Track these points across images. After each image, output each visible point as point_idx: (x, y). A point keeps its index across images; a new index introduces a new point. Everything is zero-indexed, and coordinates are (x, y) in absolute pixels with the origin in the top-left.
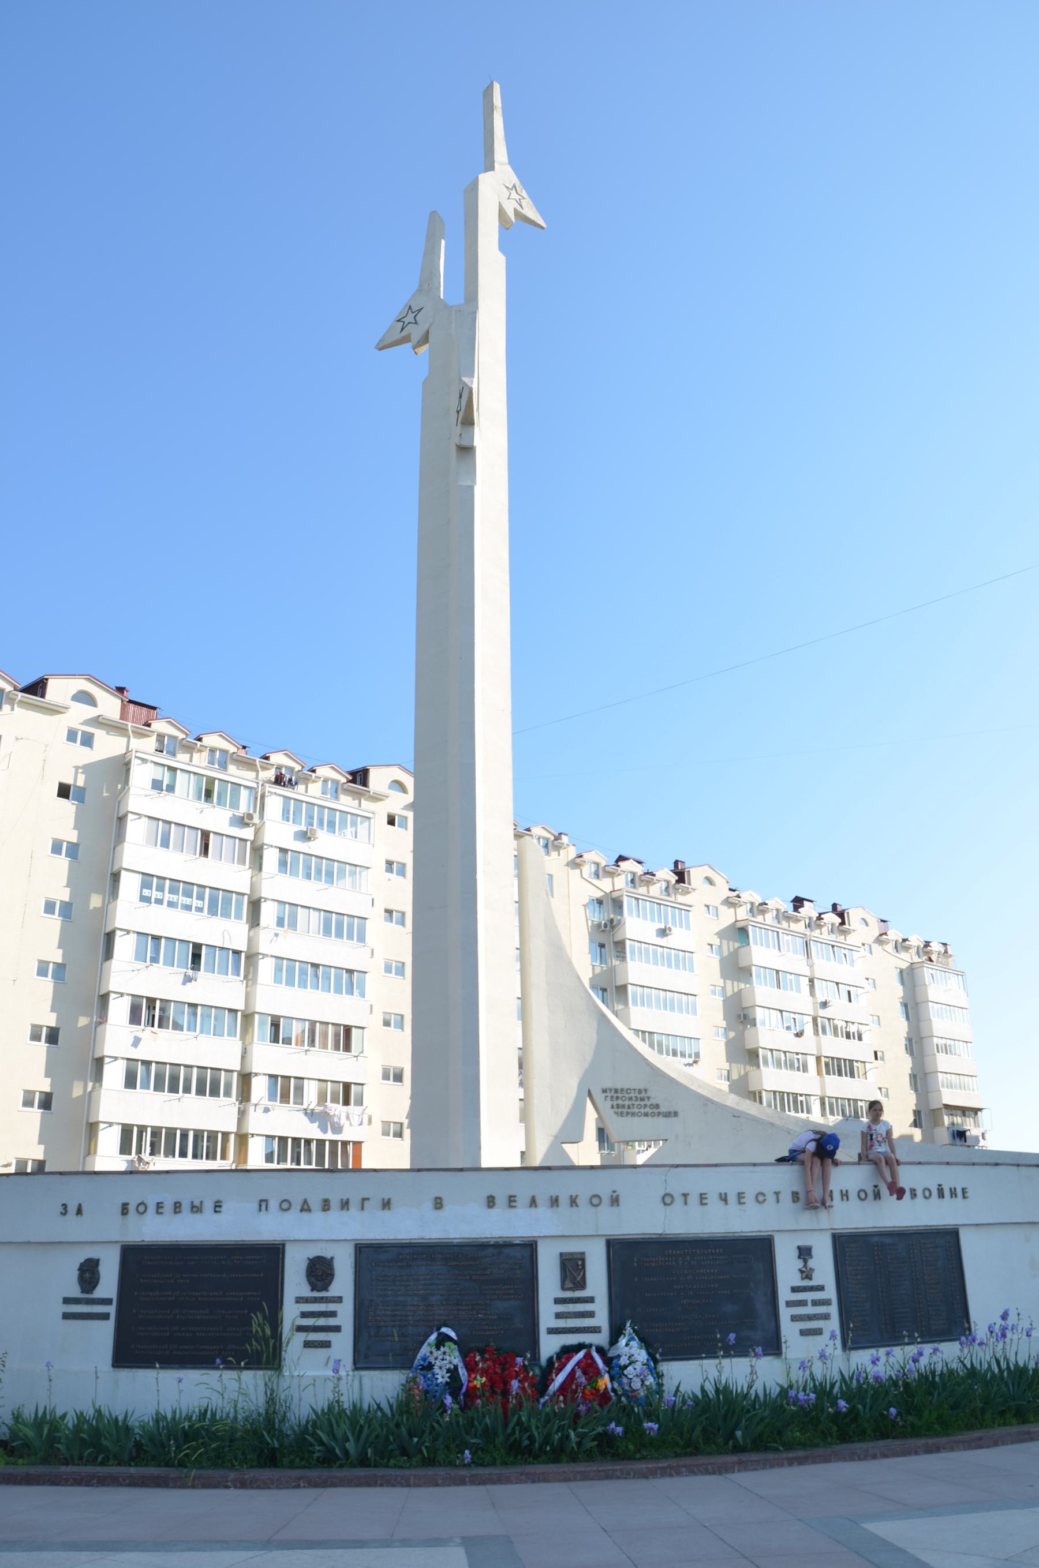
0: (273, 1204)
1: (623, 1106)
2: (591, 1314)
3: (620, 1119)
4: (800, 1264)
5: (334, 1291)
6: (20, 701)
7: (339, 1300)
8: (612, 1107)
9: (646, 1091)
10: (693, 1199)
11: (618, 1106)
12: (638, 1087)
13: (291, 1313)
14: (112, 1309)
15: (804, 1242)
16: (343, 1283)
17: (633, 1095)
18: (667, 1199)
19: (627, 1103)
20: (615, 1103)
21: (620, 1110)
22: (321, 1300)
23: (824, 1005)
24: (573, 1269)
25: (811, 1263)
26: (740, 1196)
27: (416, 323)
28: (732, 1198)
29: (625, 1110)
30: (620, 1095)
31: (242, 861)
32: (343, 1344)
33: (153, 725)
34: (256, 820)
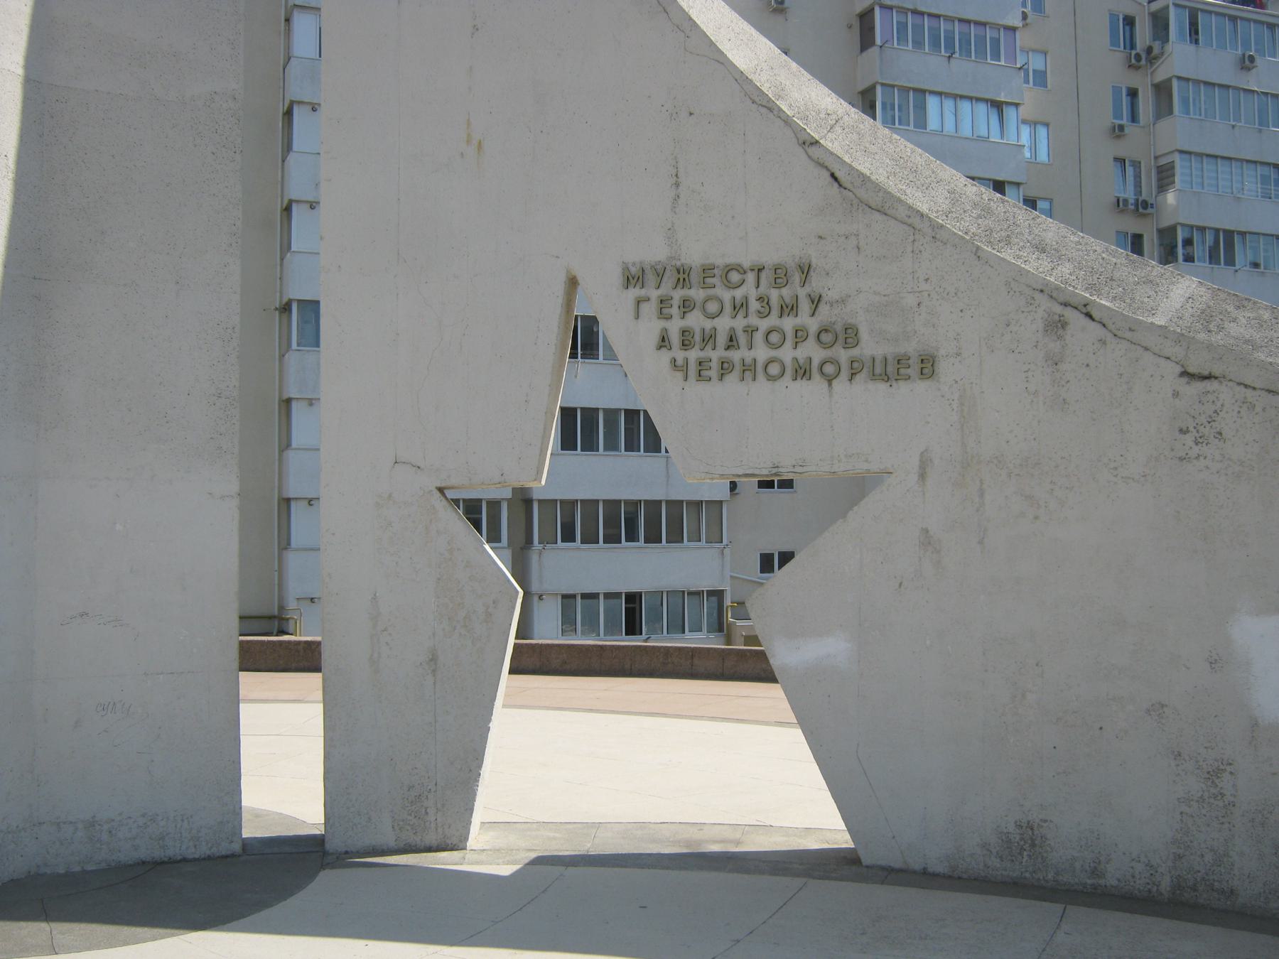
1: (709, 338)
8: (664, 342)
17: (749, 289)
19: (724, 324)
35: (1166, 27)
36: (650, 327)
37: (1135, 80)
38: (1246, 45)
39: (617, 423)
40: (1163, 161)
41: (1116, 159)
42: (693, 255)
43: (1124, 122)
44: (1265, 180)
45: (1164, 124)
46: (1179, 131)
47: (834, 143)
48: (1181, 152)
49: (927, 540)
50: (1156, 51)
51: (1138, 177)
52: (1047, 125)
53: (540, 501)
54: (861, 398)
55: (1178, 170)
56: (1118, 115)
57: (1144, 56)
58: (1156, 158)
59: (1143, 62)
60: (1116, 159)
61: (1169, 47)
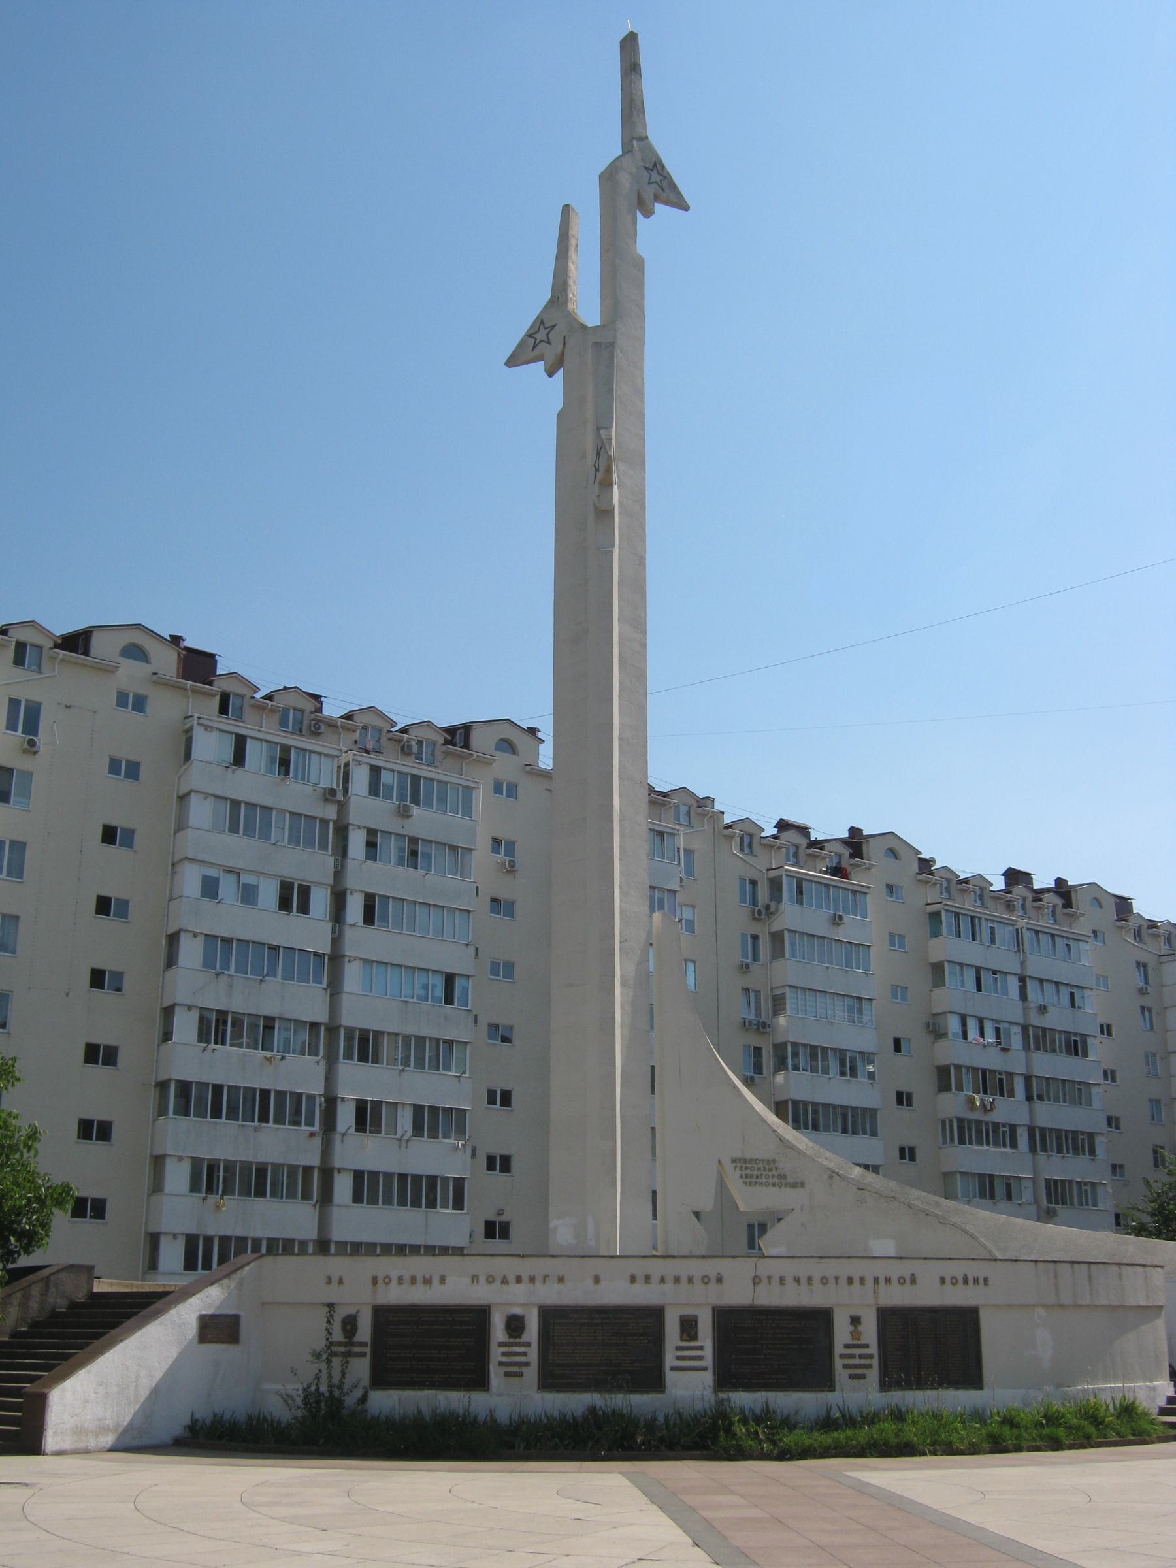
0: (482, 1279)
1: (752, 1176)
2: (700, 1358)
4: (852, 1328)
5: (525, 1337)
6: (62, 660)
7: (528, 1344)
8: (741, 1177)
9: (774, 1161)
10: (776, 1280)
11: (747, 1176)
13: (496, 1354)
14: (368, 1350)
15: (855, 1313)
16: (532, 1331)
17: (761, 1165)
18: (756, 1280)
19: (755, 1173)
20: (744, 1173)
22: (517, 1344)
23: (1042, 1009)
24: (689, 1327)
25: (860, 1328)
27: (549, 342)
28: (803, 1281)
31: (323, 846)
32: (874, 1375)
33: (215, 683)
34: (340, 797)
35: (780, 889)
36: (738, 1173)
37: (756, 928)
38: (837, 909)
39: (391, 1183)
40: (777, 992)
41: (743, 989)
42: (748, 1156)
43: (749, 960)
44: (850, 1009)
45: (778, 964)
46: (789, 971)
47: (780, 1131)
48: (790, 986)
49: (803, 1225)
50: (772, 909)
51: (758, 1002)
52: (694, 962)
53: (336, 1242)
54: (788, 1191)
55: (788, 997)
56: (745, 955)
57: (764, 911)
58: (772, 989)
59: (763, 916)
60: (743, 989)
61: (782, 906)
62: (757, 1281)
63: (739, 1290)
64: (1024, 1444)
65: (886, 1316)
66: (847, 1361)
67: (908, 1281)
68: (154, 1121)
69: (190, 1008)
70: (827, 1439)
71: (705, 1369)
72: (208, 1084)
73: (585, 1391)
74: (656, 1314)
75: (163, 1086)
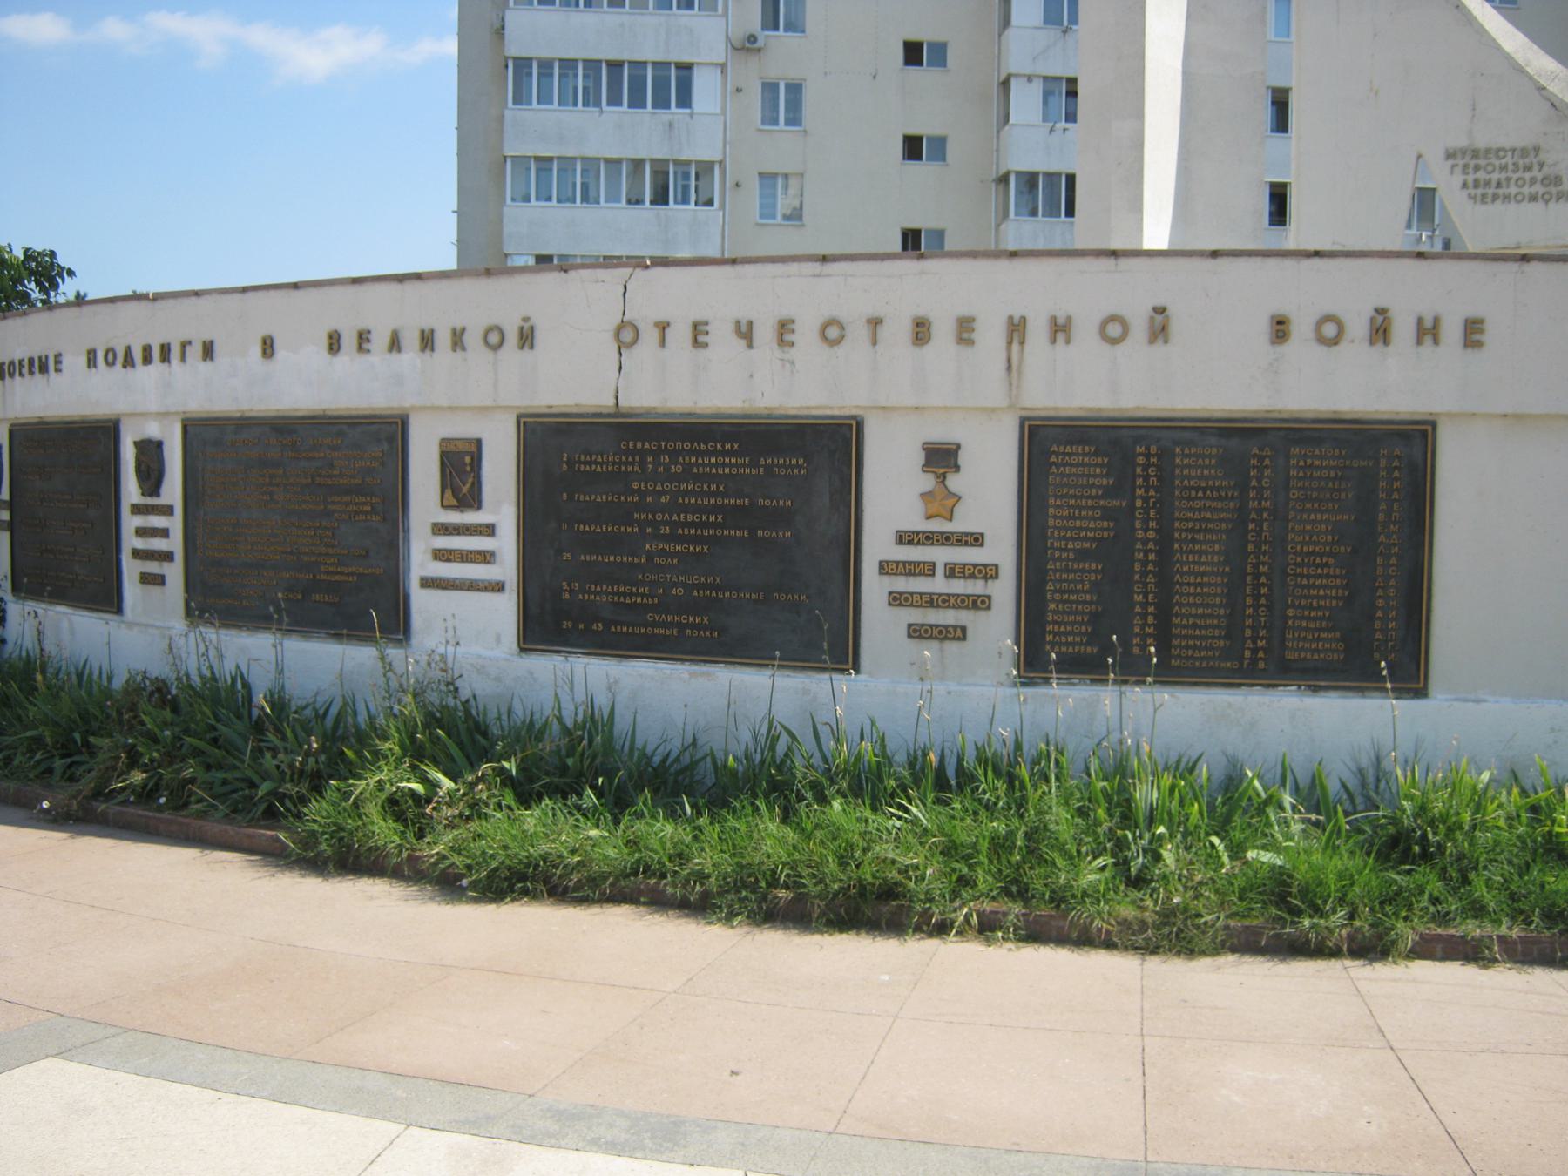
1: (1487, 183)
2: (486, 557)
3: (1481, 209)
4: (927, 482)
8: (1465, 185)
9: (1537, 150)
10: (680, 335)
11: (1476, 184)
12: (1519, 144)
15: (940, 433)
17: (1508, 160)
18: (625, 335)
19: (1495, 176)
21: (1480, 191)
24: (461, 471)
25: (954, 482)
26: (784, 328)
28: (765, 334)
29: (1490, 191)
30: (1482, 162)
32: (997, 630)
36: (1458, 179)
42: (1481, 143)
62: (627, 336)
63: (578, 374)
64: (1407, 933)
65: (1045, 444)
66: (902, 584)
67: (1139, 330)
68: (998, 226)
69: (1030, 79)
70: (594, 839)
71: (498, 587)
72: (1059, 175)
73: (257, 629)
74: (389, 433)
75: (1004, 180)
